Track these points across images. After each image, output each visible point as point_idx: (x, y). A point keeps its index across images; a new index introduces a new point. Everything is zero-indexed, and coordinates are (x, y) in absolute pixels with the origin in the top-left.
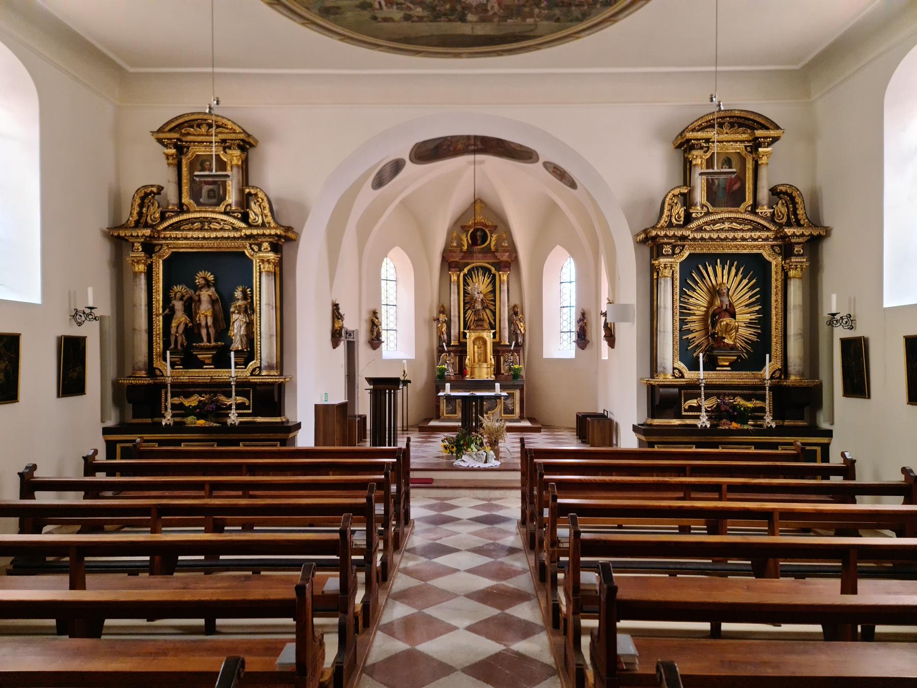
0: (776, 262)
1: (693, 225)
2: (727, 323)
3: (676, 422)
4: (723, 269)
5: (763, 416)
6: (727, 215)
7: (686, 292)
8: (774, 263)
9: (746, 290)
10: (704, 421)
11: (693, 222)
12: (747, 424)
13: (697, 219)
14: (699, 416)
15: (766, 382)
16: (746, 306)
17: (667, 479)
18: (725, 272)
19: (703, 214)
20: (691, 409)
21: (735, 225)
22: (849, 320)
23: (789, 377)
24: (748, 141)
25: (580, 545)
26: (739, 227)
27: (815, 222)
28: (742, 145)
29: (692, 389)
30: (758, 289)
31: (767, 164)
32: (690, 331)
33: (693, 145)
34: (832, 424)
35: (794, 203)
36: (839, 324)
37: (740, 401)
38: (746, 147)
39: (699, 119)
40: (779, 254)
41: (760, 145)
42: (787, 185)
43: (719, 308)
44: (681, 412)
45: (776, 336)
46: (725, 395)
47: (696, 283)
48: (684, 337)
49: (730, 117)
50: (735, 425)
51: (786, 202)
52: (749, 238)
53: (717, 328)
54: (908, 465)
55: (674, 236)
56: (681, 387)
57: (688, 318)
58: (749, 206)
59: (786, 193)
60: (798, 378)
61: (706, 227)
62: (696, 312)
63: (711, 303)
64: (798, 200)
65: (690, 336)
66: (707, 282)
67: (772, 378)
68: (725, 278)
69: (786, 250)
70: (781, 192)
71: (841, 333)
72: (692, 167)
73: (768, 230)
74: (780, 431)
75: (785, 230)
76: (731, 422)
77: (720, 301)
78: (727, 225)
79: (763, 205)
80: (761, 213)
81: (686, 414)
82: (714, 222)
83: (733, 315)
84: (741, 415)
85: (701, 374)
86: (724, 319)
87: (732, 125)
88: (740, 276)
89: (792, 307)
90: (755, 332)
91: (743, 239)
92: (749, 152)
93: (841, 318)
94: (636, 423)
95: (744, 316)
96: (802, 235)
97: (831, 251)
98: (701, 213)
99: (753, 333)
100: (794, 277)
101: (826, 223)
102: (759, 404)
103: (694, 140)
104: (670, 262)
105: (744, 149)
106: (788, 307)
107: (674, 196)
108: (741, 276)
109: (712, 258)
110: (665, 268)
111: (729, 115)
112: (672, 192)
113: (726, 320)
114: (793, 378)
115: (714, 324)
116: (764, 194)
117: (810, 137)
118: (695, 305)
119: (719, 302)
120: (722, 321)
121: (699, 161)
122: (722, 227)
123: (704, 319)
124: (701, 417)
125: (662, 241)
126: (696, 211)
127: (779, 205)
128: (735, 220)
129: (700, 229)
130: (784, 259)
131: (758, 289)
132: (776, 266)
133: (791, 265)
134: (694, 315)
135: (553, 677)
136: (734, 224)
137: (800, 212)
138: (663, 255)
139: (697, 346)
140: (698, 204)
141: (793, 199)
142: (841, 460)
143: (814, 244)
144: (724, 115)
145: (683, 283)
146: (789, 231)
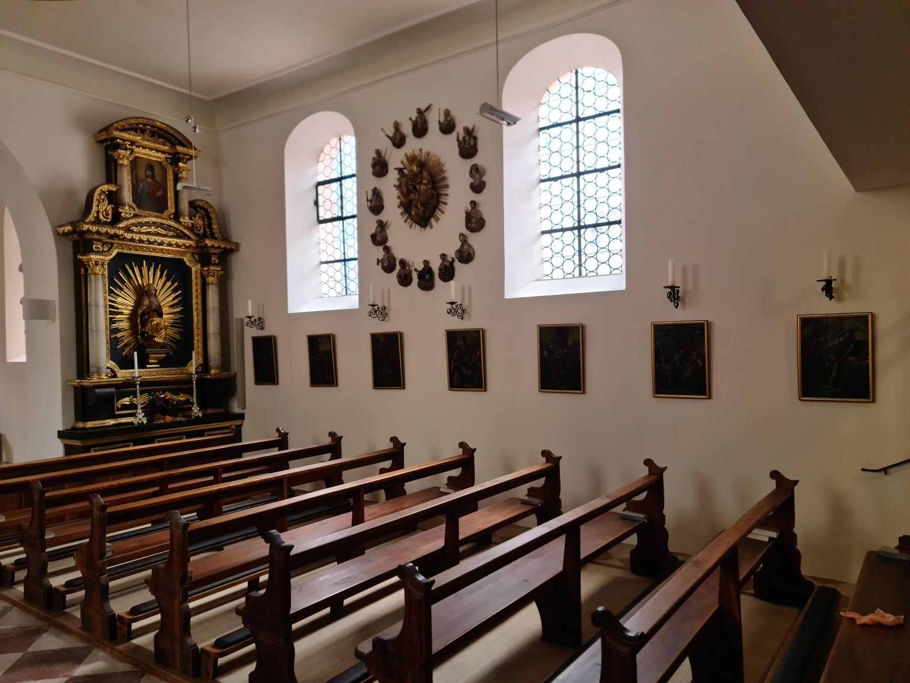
0: (195, 269)
1: (122, 225)
2: (158, 323)
3: (111, 422)
4: (149, 270)
5: (191, 408)
6: (154, 220)
7: (113, 290)
8: (194, 269)
9: (169, 292)
10: (140, 418)
11: (122, 222)
12: (178, 416)
13: (127, 219)
14: (135, 413)
15: (193, 376)
16: (170, 306)
17: (172, 472)
18: (151, 273)
19: (132, 215)
20: (124, 407)
21: (160, 230)
22: (260, 323)
23: (210, 371)
24: (169, 154)
25: (187, 536)
26: (164, 232)
27: (225, 238)
28: (163, 156)
29: (127, 387)
30: (180, 292)
31: (186, 178)
32: (118, 330)
33: (118, 144)
34: (244, 408)
35: (210, 219)
36: (253, 325)
37: (169, 396)
38: (166, 158)
39: (124, 120)
40: (198, 262)
41: (179, 160)
42: (204, 201)
43: (148, 308)
44: (114, 412)
45: (198, 335)
46: (156, 391)
47: (123, 282)
48: (113, 336)
49: (151, 126)
50: (169, 419)
51: (202, 216)
52: (146, 241)
53: (147, 327)
54: (332, 430)
55: (107, 233)
56: (117, 386)
57: (116, 317)
58: (172, 214)
59: (202, 208)
60: (217, 372)
61: (133, 228)
62: (124, 311)
63: (138, 303)
64: (213, 216)
65: (119, 335)
66: (133, 281)
67: (197, 372)
68: (151, 278)
69: (204, 257)
70: (199, 207)
71: (251, 333)
72: (118, 167)
73: (189, 238)
74: (205, 419)
75: (206, 241)
76: (165, 416)
77: (149, 301)
78: (153, 229)
79: (185, 216)
80: (184, 222)
81: (119, 412)
82: (141, 225)
83: (160, 315)
84: (168, 408)
85: (136, 372)
86: (154, 319)
87: (153, 134)
88: (164, 278)
89: (211, 309)
90: (178, 331)
91: (141, 241)
92: (169, 163)
93: (255, 320)
94: (61, 429)
95: (168, 317)
96: (219, 247)
97: (241, 264)
98: (130, 214)
99: (176, 331)
100: (212, 283)
101: (235, 239)
102: (182, 397)
103: (120, 139)
104: (101, 259)
105: (165, 159)
106: (207, 309)
107: (103, 192)
108: (165, 278)
109: (139, 260)
110: (97, 265)
111: (151, 124)
112: (101, 188)
113: (156, 320)
114: (213, 371)
115: (144, 323)
116: (184, 206)
117: (217, 162)
118: (122, 304)
119: (147, 301)
120: (153, 321)
121: (126, 162)
122: (148, 230)
123: (132, 317)
124: (137, 415)
125: (92, 237)
126: (125, 211)
127: (197, 217)
128: (161, 225)
129: (128, 229)
130: (202, 266)
131: (180, 292)
132: (196, 272)
133: (210, 273)
134: (122, 313)
135: (143, 678)
136: (160, 229)
137: (215, 227)
138: (94, 252)
139: (126, 345)
140: (126, 205)
141: (207, 214)
142: (277, 434)
143: (227, 254)
144: (147, 123)
145: (112, 282)
146: (209, 242)
